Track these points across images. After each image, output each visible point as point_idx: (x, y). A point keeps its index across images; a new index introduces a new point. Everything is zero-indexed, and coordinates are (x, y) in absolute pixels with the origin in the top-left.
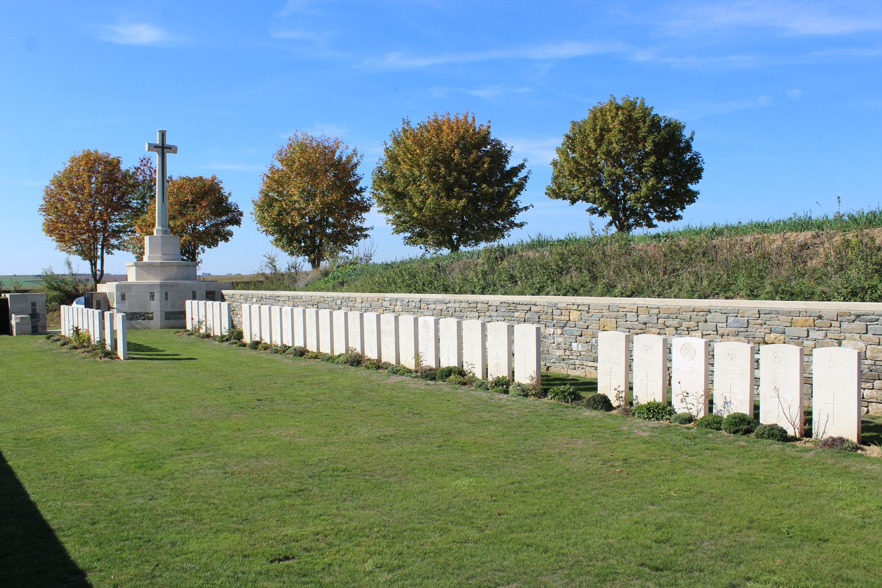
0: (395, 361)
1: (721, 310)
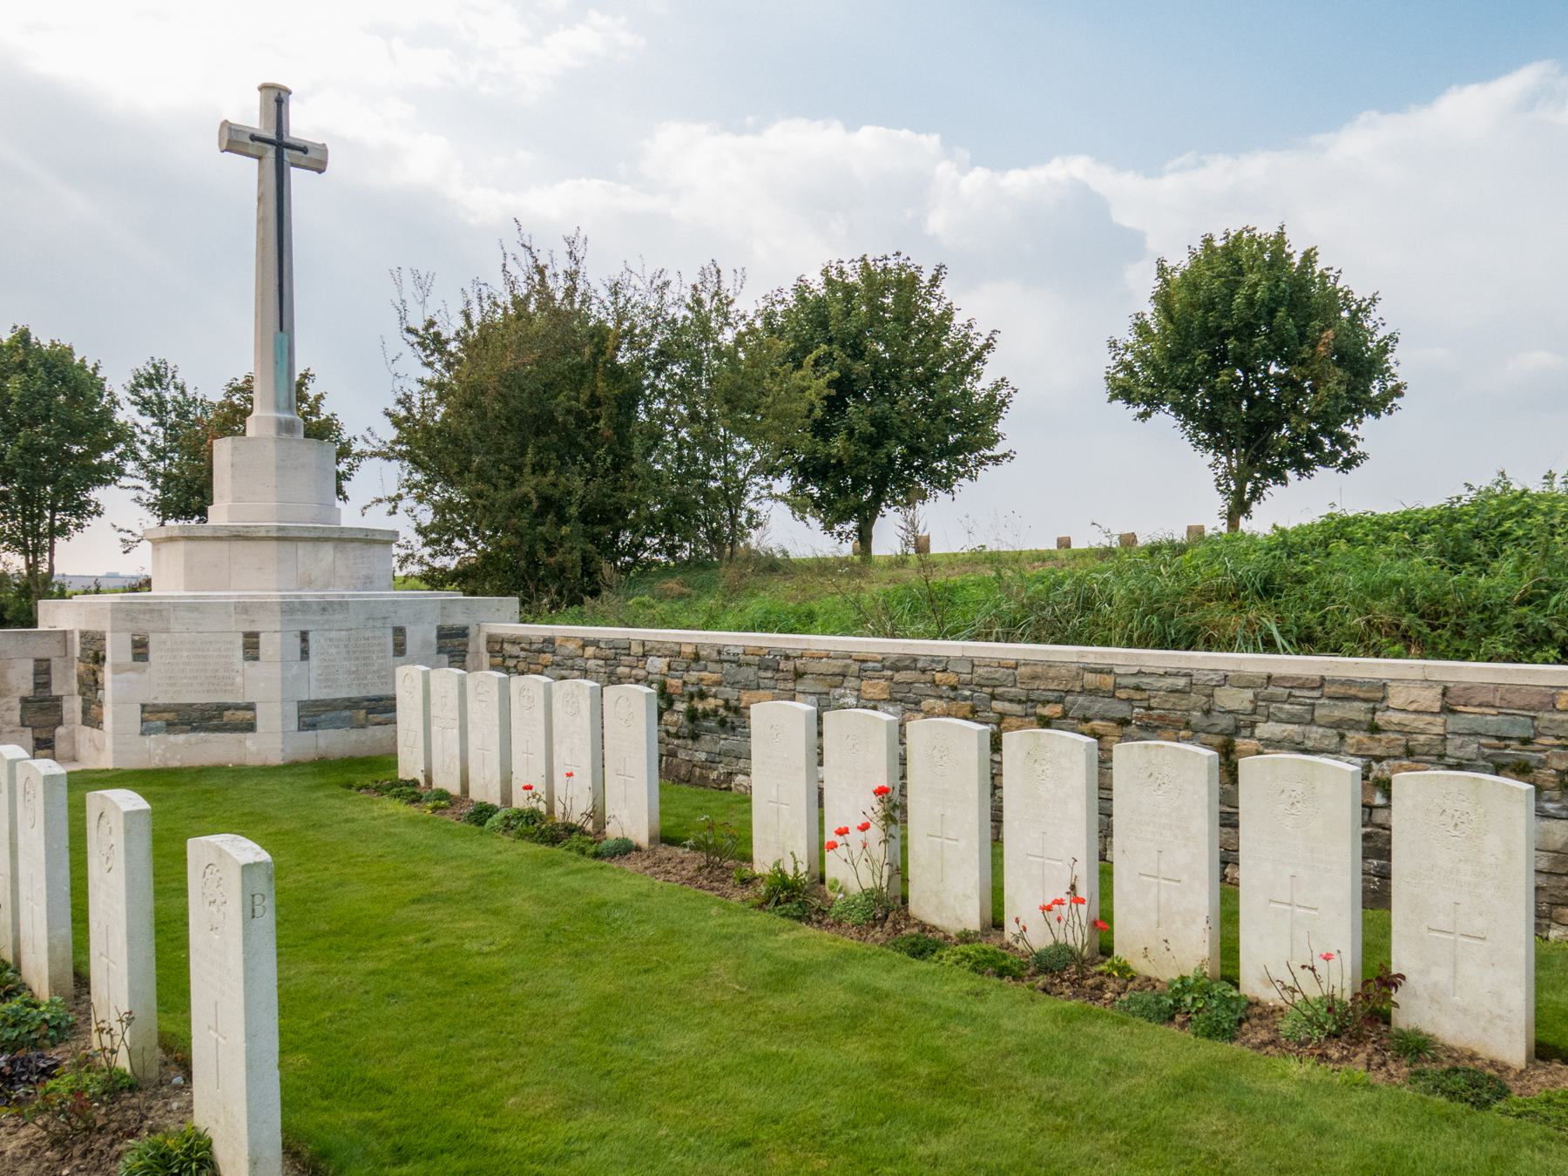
0: (499, 795)
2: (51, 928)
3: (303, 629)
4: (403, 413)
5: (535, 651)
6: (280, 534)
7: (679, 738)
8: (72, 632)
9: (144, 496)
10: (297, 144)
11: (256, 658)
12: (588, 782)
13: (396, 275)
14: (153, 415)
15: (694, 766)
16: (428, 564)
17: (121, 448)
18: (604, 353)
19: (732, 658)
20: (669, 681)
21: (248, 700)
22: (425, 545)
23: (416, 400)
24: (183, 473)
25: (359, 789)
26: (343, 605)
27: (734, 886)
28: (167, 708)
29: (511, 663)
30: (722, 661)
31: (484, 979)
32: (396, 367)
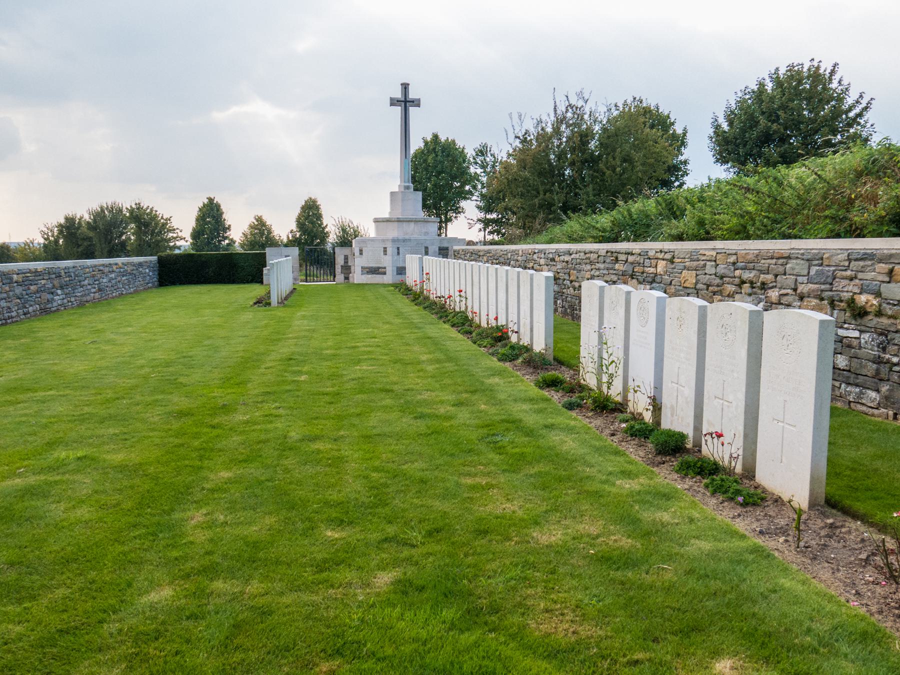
1: (803, 254)
26: (410, 240)
28: (367, 268)
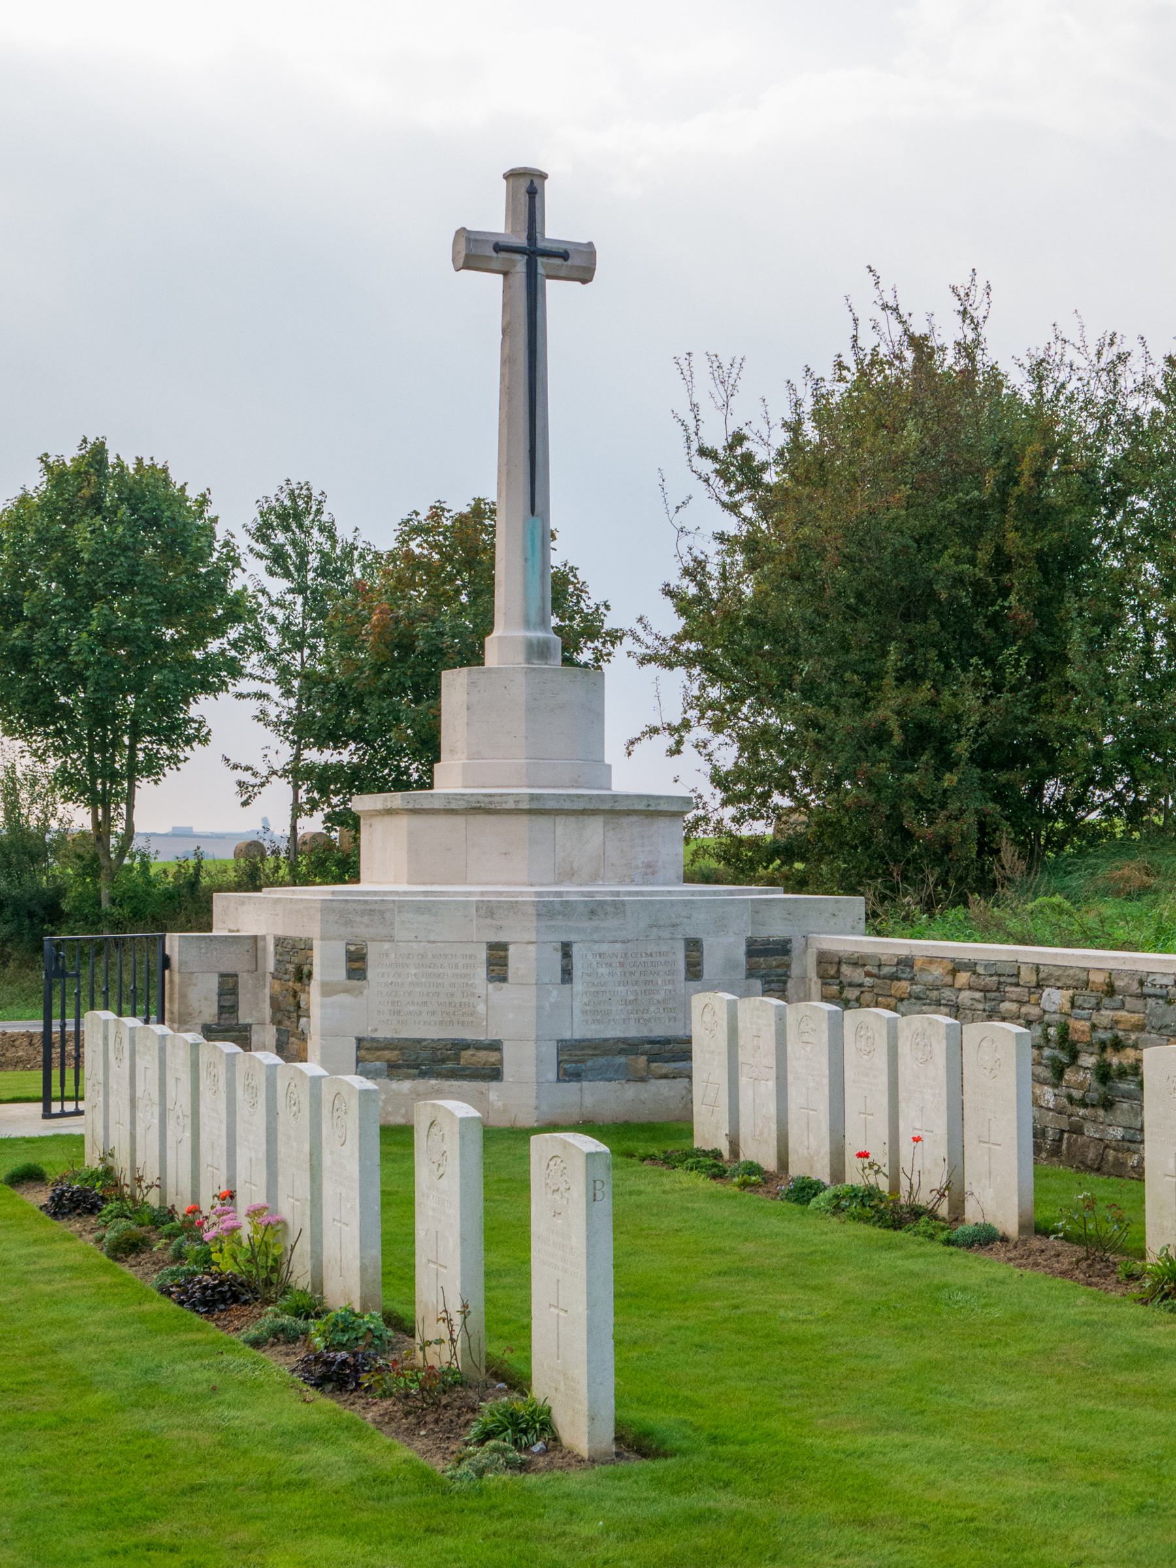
0: (828, 1170)
2: (363, 1247)
3: (565, 939)
4: (692, 590)
5: (885, 977)
6: (535, 806)
7: (1085, 1106)
8: (264, 938)
9: (273, 712)
10: (554, 247)
11: (504, 979)
12: (943, 1151)
13: (684, 366)
14: (287, 575)
15: (1107, 1147)
16: (730, 834)
17: (234, 632)
18: (1017, 483)
19: (1158, 991)
20: (1072, 1023)
21: (492, 1036)
22: (724, 803)
23: (713, 569)
24: (332, 671)
25: (643, 1159)
26: (618, 907)
27: (1118, 1282)
29: (851, 994)
30: (1144, 996)
31: (797, 1341)
32: (683, 518)
